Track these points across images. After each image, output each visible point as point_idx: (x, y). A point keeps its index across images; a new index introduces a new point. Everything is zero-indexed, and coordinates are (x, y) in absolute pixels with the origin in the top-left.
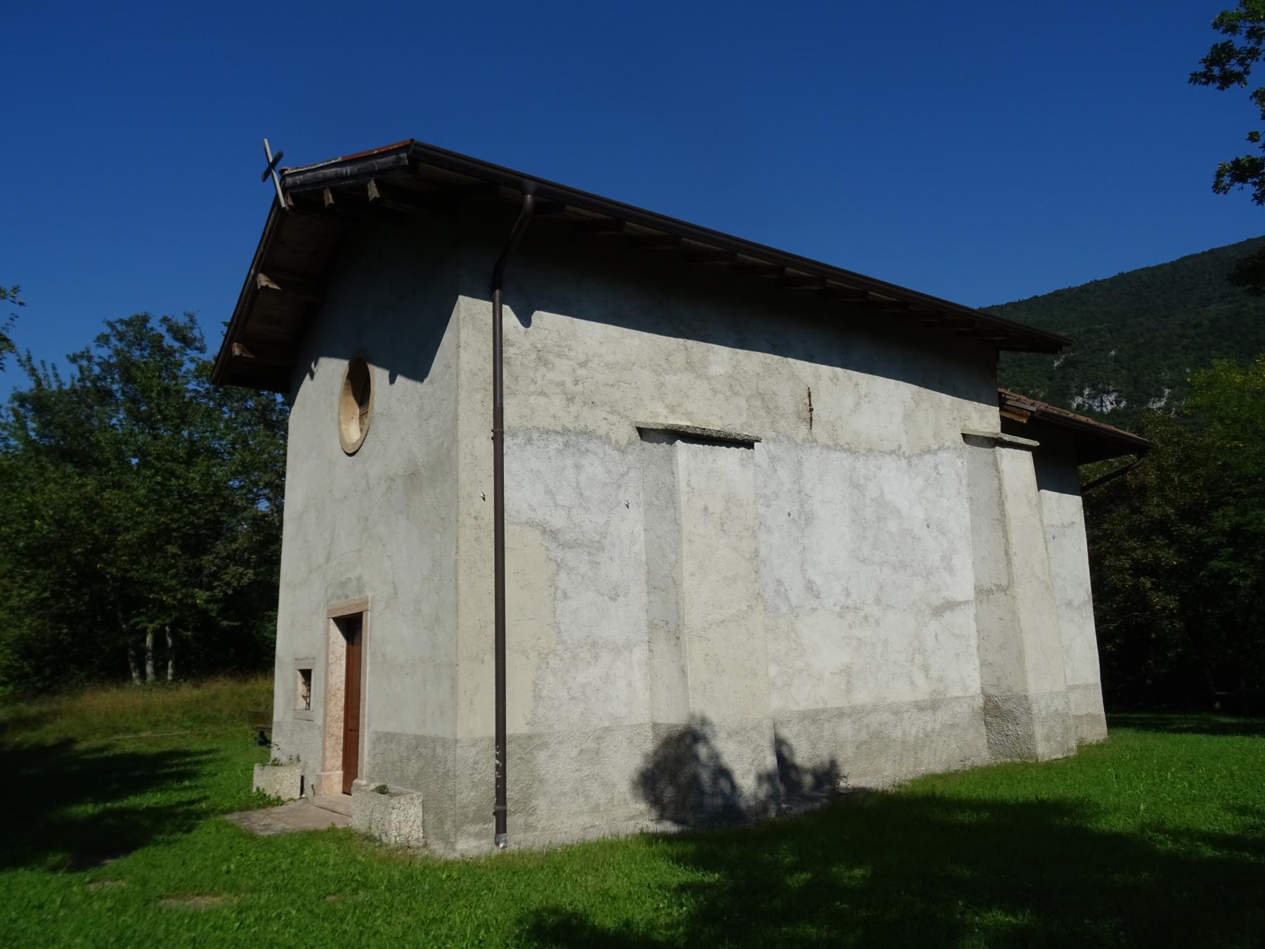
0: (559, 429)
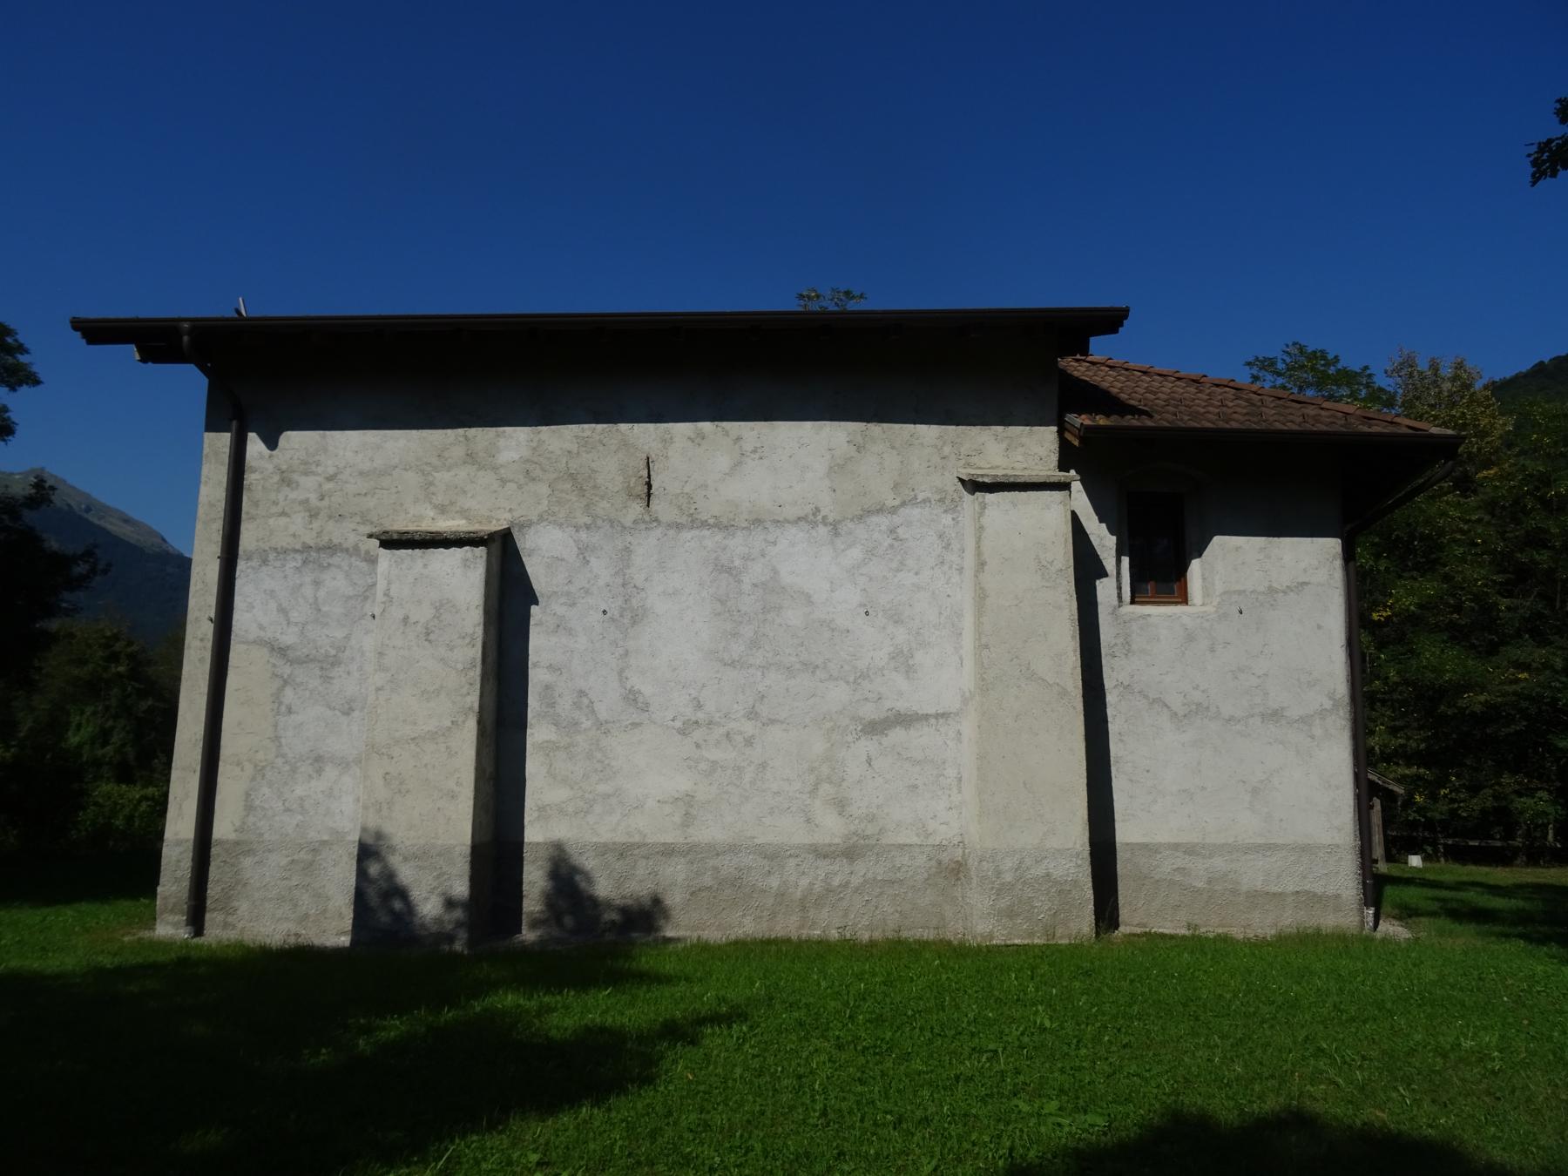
0: (298, 547)
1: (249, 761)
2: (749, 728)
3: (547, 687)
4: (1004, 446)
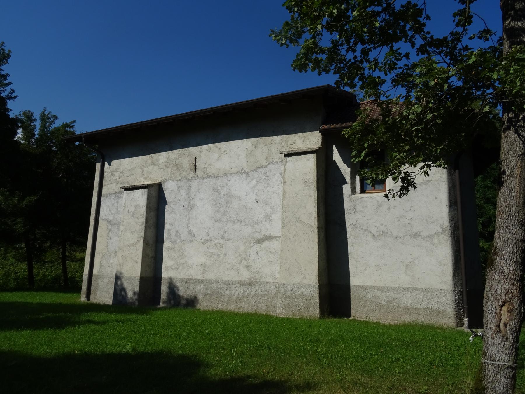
0: (114, 192)
1: (101, 253)
2: (222, 242)
3: (169, 230)
4: (302, 140)
